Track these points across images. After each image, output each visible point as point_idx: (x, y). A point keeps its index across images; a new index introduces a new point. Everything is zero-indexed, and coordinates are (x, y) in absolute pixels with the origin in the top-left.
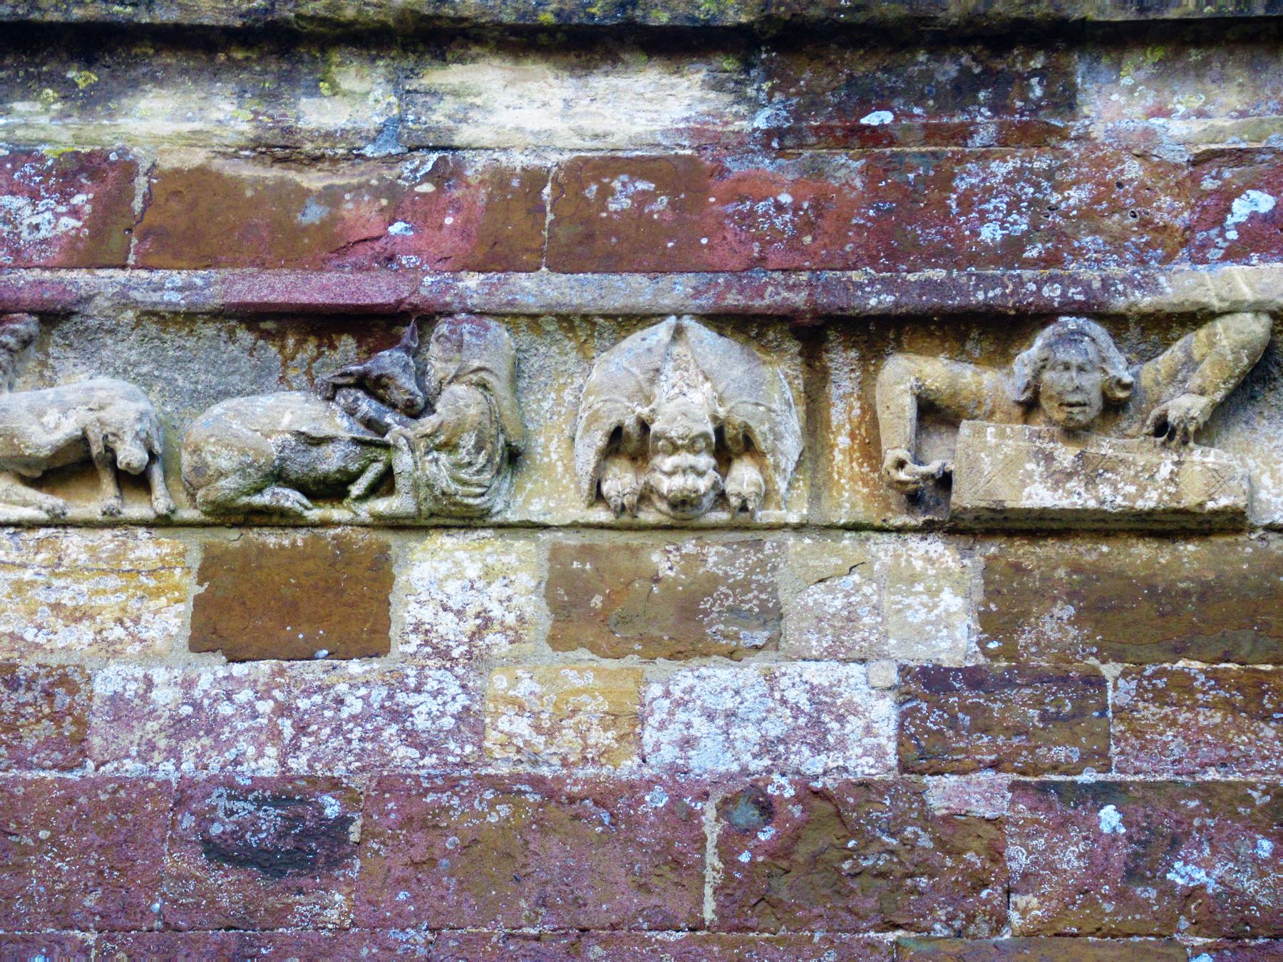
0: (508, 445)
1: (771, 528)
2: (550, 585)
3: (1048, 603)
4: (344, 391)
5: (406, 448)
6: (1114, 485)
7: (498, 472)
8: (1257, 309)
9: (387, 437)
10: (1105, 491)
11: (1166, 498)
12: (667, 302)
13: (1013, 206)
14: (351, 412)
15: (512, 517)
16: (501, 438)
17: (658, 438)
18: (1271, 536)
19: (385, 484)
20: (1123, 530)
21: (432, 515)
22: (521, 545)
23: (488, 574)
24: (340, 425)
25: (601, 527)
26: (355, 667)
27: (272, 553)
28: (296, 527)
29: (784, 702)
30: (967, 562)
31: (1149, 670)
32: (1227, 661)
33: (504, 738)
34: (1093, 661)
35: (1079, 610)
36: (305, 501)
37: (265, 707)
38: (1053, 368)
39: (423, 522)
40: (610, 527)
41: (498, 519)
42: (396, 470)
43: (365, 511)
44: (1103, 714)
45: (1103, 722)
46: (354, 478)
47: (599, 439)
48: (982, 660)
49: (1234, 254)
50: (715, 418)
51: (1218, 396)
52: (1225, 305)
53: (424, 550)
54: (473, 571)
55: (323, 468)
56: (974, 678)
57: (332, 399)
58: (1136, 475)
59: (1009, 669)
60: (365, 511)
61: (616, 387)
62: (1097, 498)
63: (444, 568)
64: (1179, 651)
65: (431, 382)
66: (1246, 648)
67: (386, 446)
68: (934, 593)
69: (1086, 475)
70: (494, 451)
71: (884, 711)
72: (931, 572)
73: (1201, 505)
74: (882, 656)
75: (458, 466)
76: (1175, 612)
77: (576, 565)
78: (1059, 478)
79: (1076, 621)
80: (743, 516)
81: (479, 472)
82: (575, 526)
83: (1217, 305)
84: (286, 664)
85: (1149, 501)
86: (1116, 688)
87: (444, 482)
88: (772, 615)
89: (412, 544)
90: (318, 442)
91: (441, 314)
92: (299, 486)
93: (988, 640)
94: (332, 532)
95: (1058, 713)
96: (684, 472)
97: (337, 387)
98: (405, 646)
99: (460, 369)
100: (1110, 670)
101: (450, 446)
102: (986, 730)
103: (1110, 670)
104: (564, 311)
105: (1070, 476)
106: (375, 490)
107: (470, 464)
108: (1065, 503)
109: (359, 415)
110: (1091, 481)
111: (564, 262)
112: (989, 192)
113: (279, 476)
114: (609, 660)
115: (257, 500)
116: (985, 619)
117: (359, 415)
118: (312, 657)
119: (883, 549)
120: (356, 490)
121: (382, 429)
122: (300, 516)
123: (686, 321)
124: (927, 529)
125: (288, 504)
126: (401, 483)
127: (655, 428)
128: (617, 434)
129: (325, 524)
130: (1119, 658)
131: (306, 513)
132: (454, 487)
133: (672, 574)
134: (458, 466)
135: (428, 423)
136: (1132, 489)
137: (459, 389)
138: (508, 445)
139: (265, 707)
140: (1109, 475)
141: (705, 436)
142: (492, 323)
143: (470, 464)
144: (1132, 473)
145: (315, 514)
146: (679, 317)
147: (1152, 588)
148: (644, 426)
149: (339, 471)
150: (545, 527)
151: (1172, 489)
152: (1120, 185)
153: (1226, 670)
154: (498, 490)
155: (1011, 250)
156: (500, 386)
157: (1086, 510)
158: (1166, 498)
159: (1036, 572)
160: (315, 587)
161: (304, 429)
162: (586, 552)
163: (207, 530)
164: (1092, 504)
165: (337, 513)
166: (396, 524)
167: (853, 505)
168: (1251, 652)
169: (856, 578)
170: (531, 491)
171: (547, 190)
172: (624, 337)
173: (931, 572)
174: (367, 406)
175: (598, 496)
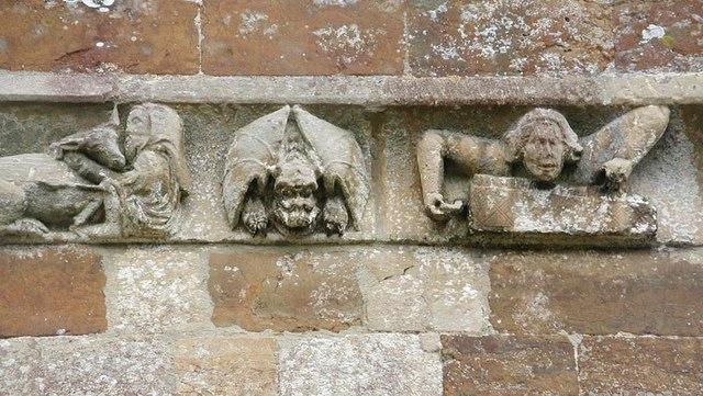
0: (181, 189)
1: (352, 243)
2: (210, 281)
3: (532, 293)
4: (71, 154)
5: (114, 193)
6: (572, 216)
7: (175, 208)
8: (661, 103)
9: (101, 185)
10: (566, 221)
11: (605, 225)
12: (283, 96)
13: (501, 32)
14: (75, 169)
15: (184, 238)
16: (177, 185)
17: (281, 186)
18: (671, 249)
19: (99, 217)
20: (132, 244)
21: (130, 236)
22: (189, 255)
23: (169, 276)
24: (67, 178)
25: (242, 243)
26: (84, 340)
27: (21, 262)
28: (37, 244)
29: (369, 361)
30: (478, 265)
31: (600, 338)
32: (649, 333)
33: (187, 388)
34: (563, 332)
35: (551, 298)
36: (45, 228)
37: (25, 369)
38: (533, 142)
39: (124, 241)
40: (248, 244)
41: (175, 238)
42: (107, 207)
43: (84, 234)
44: (573, 369)
45: (572, 373)
46: (76, 212)
47: (243, 187)
48: (494, 332)
49: (645, 64)
50: (317, 172)
51: (636, 160)
52: (640, 101)
53: (126, 259)
54: (159, 274)
55: (58, 206)
56: (490, 344)
57: (61, 159)
58: (586, 211)
59: (510, 337)
60: (84, 234)
61: (252, 152)
62: (562, 226)
63: (139, 271)
64: (618, 328)
65: (130, 147)
66: (660, 323)
67: (101, 191)
68: (459, 287)
69: (554, 210)
70: (173, 194)
71: (435, 367)
72: (457, 272)
73: (627, 230)
74: (429, 329)
75: (149, 205)
76: (614, 300)
77: (227, 269)
78: (537, 213)
79: (550, 306)
80: (335, 237)
81: (162, 209)
82: (224, 243)
83: (635, 100)
84: (37, 339)
85: (595, 227)
86: (579, 351)
87: (141, 215)
88: (356, 300)
89: (117, 255)
90: (53, 189)
91: (134, 103)
92: (39, 218)
93: (496, 319)
94: (62, 247)
95: (544, 368)
96: (299, 208)
97: (65, 152)
98: (117, 323)
99: (150, 140)
100: (575, 339)
101: (144, 192)
102: (500, 379)
103: (575, 339)
104: (216, 101)
105: (544, 211)
106: (90, 221)
107: (157, 203)
108: (542, 229)
109: (81, 170)
110: (557, 214)
111: (216, 68)
112: (484, 23)
113: (28, 213)
114: (253, 333)
115: (12, 227)
116: (492, 303)
117: (81, 170)
118: (54, 334)
119: (425, 257)
120: (79, 220)
121: (96, 180)
122: (40, 237)
123: (297, 109)
124: (452, 244)
125: (33, 230)
126: (109, 215)
127: (280, 179)
128: (254, 183)
129: (57, 242)
130: (580, 332)
131: (44, 235)
132: (146, 218)
133: (290, 274)
134: (149, 205)
135: (130, 176)
136: (584, 219)
137: (150, 154)
138: (181, 189)
139: (25, 369)
140: (568, 210)
141: (311, 186)
142: (167, 109)
143: (157, 203)
144: (583, 209)
145: (50, 235)
146: (291, 106)
147: (597, 284)
148: (271, 178)
149: (68, 208)
150: (205, 243)
151: (609, 220)
152: (567, 19)
153: (648, 339)
154: (174, 219)
155: (502, 64)
156: (175, 150)
157: (554, 234)
158: (605, 225)
159: (523, 272)
160: (52, 285)
161: (44, 180)
162: (232, 261)
163: (181, 248)
164: (558, 229)
165: (65, 236)
166: (107, 244)
167: (404, 228)
168: (664, 327)
169: (408, 276)
170: (195, 219)
171: (198, 19)
172: (255, 119)
173: (457, 272)
174: (87, 165)
175: (239, 224)
